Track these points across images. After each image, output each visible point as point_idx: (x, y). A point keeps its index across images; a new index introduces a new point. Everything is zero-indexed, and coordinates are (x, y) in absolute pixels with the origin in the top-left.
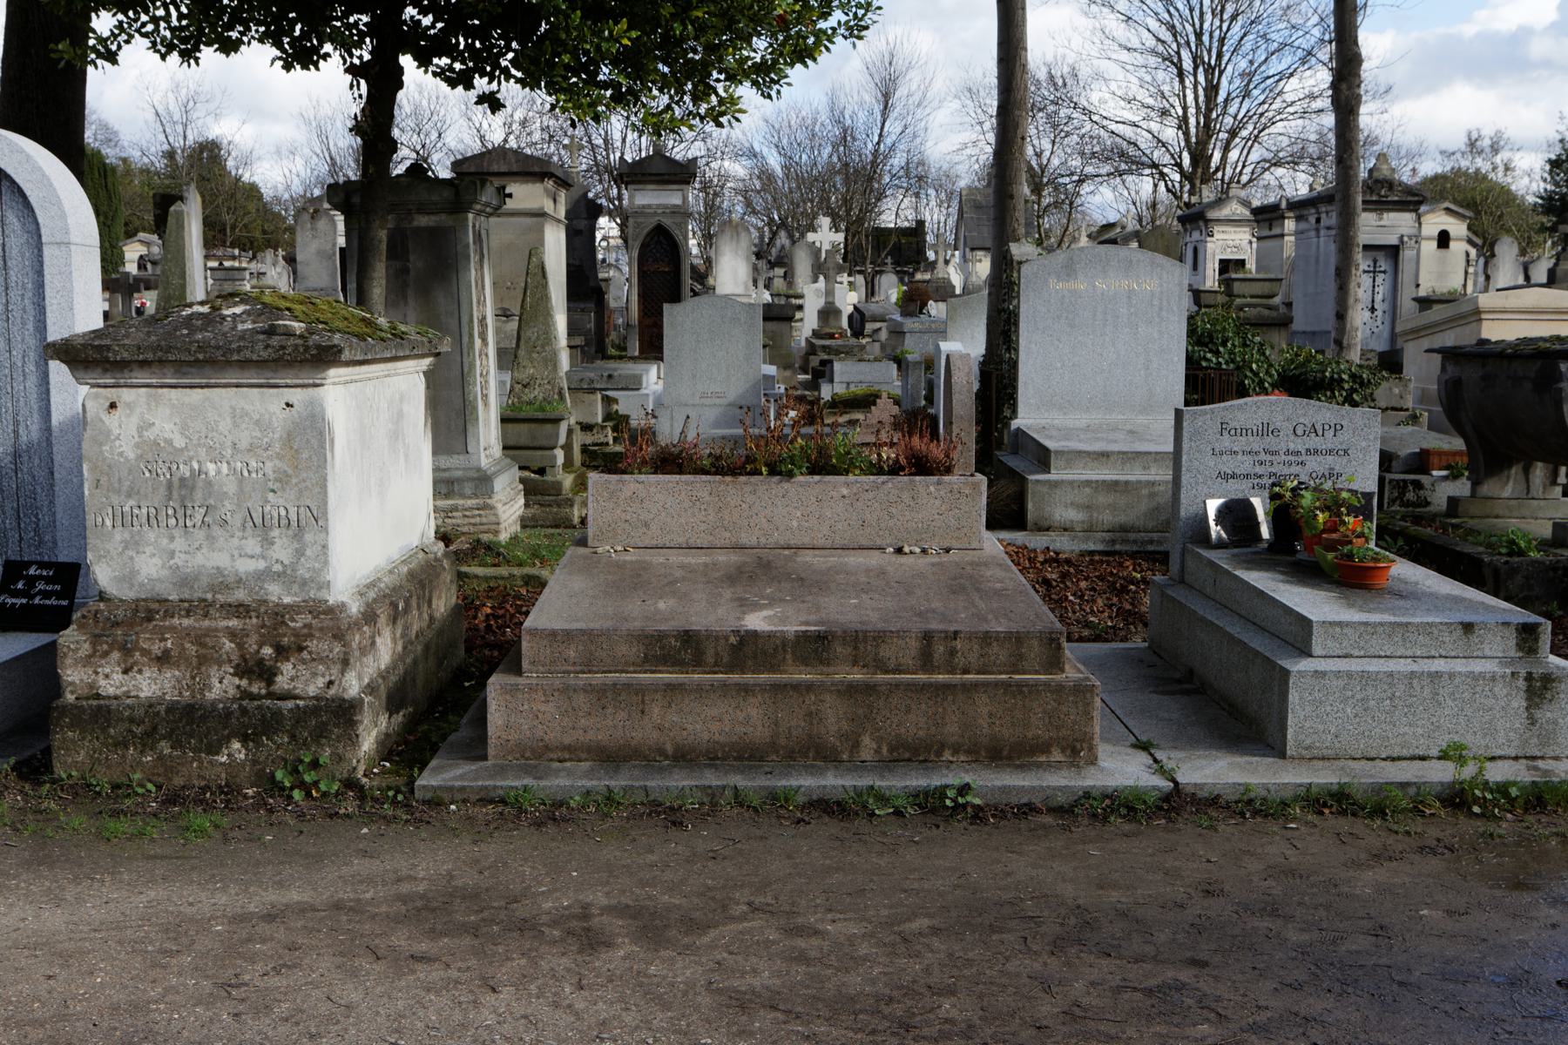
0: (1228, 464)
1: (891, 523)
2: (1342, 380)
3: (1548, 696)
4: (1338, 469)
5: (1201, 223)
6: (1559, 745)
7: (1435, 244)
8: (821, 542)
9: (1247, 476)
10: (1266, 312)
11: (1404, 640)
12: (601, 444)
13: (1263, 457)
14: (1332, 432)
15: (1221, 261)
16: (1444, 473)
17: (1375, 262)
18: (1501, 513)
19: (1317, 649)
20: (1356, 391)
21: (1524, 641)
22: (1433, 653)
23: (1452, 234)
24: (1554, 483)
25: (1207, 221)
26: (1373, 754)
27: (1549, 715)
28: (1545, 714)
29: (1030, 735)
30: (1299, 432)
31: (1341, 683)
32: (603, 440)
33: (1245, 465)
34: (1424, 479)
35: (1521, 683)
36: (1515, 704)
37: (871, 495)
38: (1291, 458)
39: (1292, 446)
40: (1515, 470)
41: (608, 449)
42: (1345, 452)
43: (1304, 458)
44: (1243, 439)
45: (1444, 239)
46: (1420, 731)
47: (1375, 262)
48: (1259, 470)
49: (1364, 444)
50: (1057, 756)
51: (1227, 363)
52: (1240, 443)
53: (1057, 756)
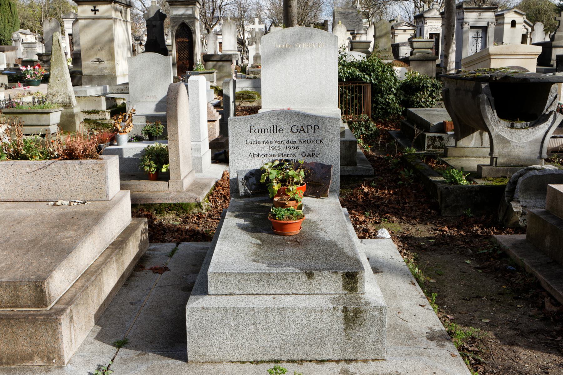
0: (255, 149)
1: (56, 187)
2: (428, 87)
3: (359, 322)
4: (317, 150)
5: (422, 19)
6: (367, 352)
7: (510, 25)
8: (18, 198)
9: (266, 156)
10: (427, 55)
11: (268, 283)
12: (103, 119)
13: (274, 144)
14: (313, 130)
15: (430, 34)
17: (477, 33)
18: (468, 155)
19: (211, 290)
20: (434, 91)
21: (348, 283)
22: (288, 292)
23: (517, 22)
25: (424, 18)
26: (244, 359)
27: (359, 334)
28: (357, 333)
29: (19, 349)
30: (294, 130)
31: (220, 315)
32: (104, 117)
35: (340, 314)
36: (336, 327)
37: (42, 171)
38: (291, 145)
39: (290, 139)
40: (476, 134)
41: (106, 122)
43: (298, 145)
44: (263, 135)
45: (513, 24)
46: (275, 344)
47: (477, 33)
48: (272, 152)
49: (331, 137)
50: (38, 362)
51: (374, 80)
52: (261, 137)
53: (38, 362)
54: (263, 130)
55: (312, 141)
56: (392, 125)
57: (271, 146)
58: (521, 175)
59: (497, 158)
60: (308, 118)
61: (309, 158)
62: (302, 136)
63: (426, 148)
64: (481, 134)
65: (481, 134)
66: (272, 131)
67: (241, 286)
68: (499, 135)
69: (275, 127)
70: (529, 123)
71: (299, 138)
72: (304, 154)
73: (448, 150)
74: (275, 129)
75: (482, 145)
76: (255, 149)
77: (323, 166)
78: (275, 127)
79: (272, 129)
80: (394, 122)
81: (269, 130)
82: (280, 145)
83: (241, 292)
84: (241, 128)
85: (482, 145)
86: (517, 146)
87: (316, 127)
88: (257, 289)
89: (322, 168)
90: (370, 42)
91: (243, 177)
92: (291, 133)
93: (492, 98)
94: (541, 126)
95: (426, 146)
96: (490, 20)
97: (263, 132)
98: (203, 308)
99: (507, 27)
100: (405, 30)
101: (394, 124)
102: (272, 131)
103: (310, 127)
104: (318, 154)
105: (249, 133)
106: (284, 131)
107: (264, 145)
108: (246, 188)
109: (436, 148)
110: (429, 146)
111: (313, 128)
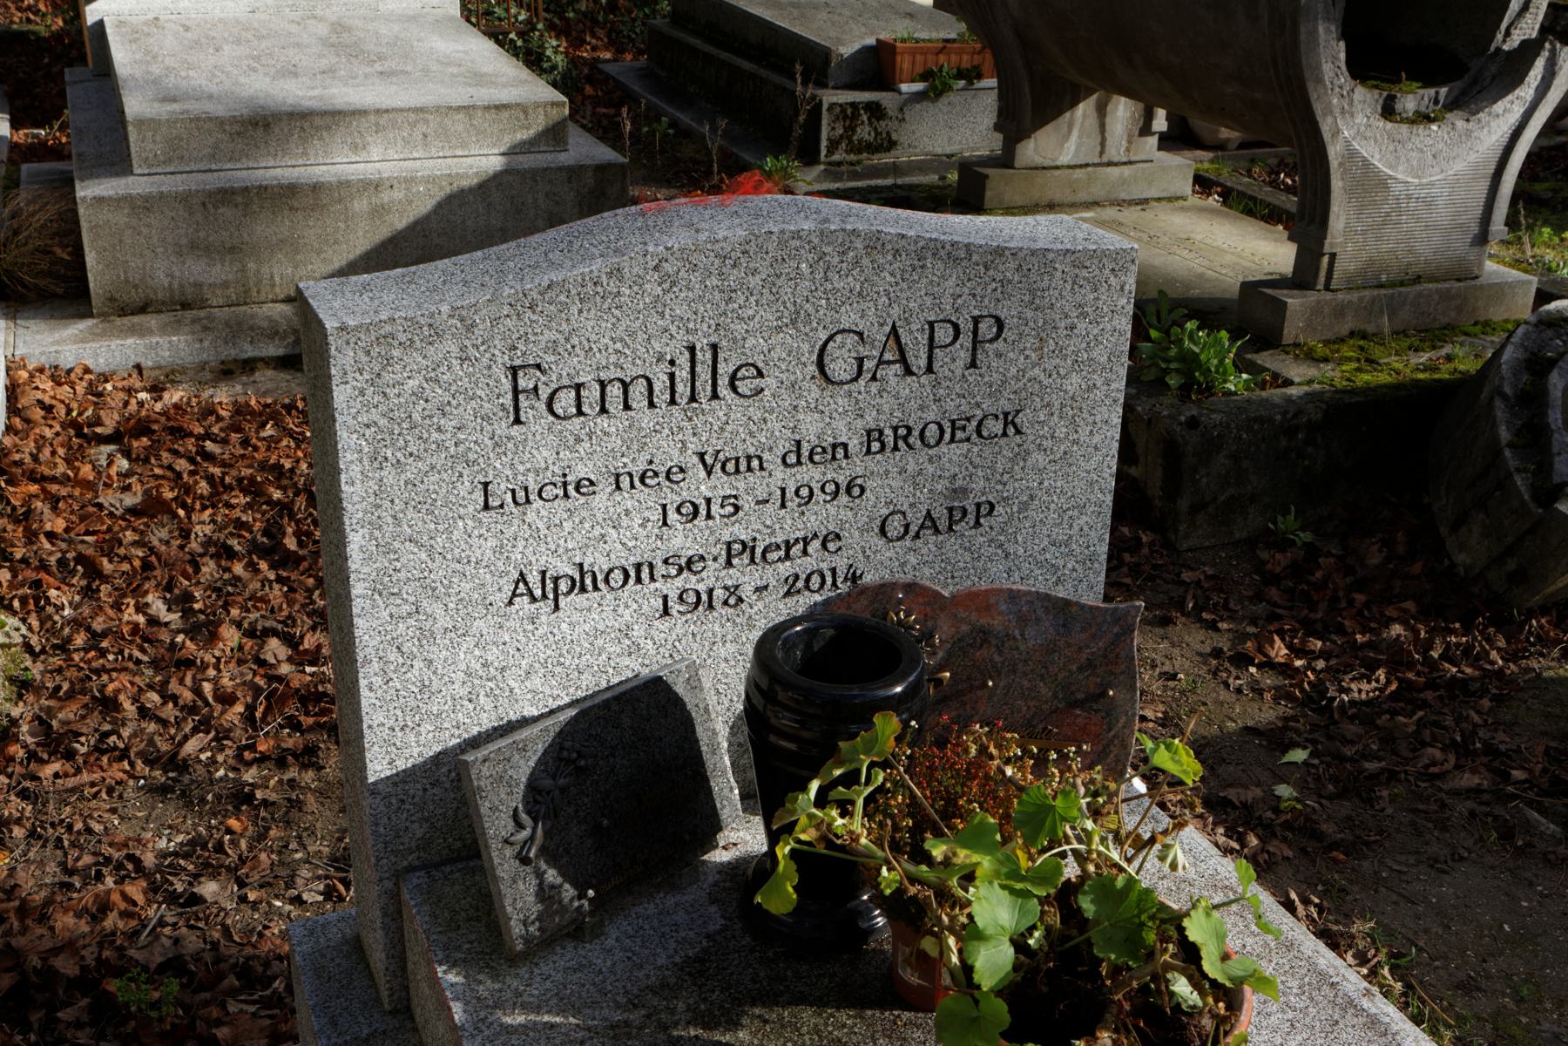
0: (554, 539)
9: (638, 572)
13: (699, 486)
16: (918, 86)
24: (1146, 130)
30: (840, 367)
33: (624, 528)
34: (884, 98)
38: (811, 474)
39: (811, 429)
40: (1084, 110)
42: (1009, 420)
43: (857, 466)
48: (682, 540)
49: (1074, 382)
52: (606, 442)
54: (615, 391)
55: (953, 430)
56: (594, 36)
57: (672, 499)
59: (1333, 256)
60: (934, 267)
62: (887, 403)
63: (823, 152)
64: (1101, 110)
65: (1101, 110)
66: (682, 389)
68: (1352, 154)
69: (704, 356)
70: (1444, 91)
71: (870, 420)
73: (989, 184)
74: (704, 373)
75: (1102, 153)
76: (554, 539)
78: (704, 356)
79: (683, 374)
80: (595, 22)
81: (661, 383)
84: (438, 394)
85: (1102, 153)
86: (1409, 197)
91: (517, 800)
92: (813, 392)
94: (1499, 107)
95: (824, 143)
97: (615, 404)
101: (601, 33)
102: (682, 389)
103: (943, 334)
105: (502, 427)
106: (770, 382)
107: (627, 500)
108: (552, 875)
109: (860, 152)
110: (833, 145)
111: (966, 340)
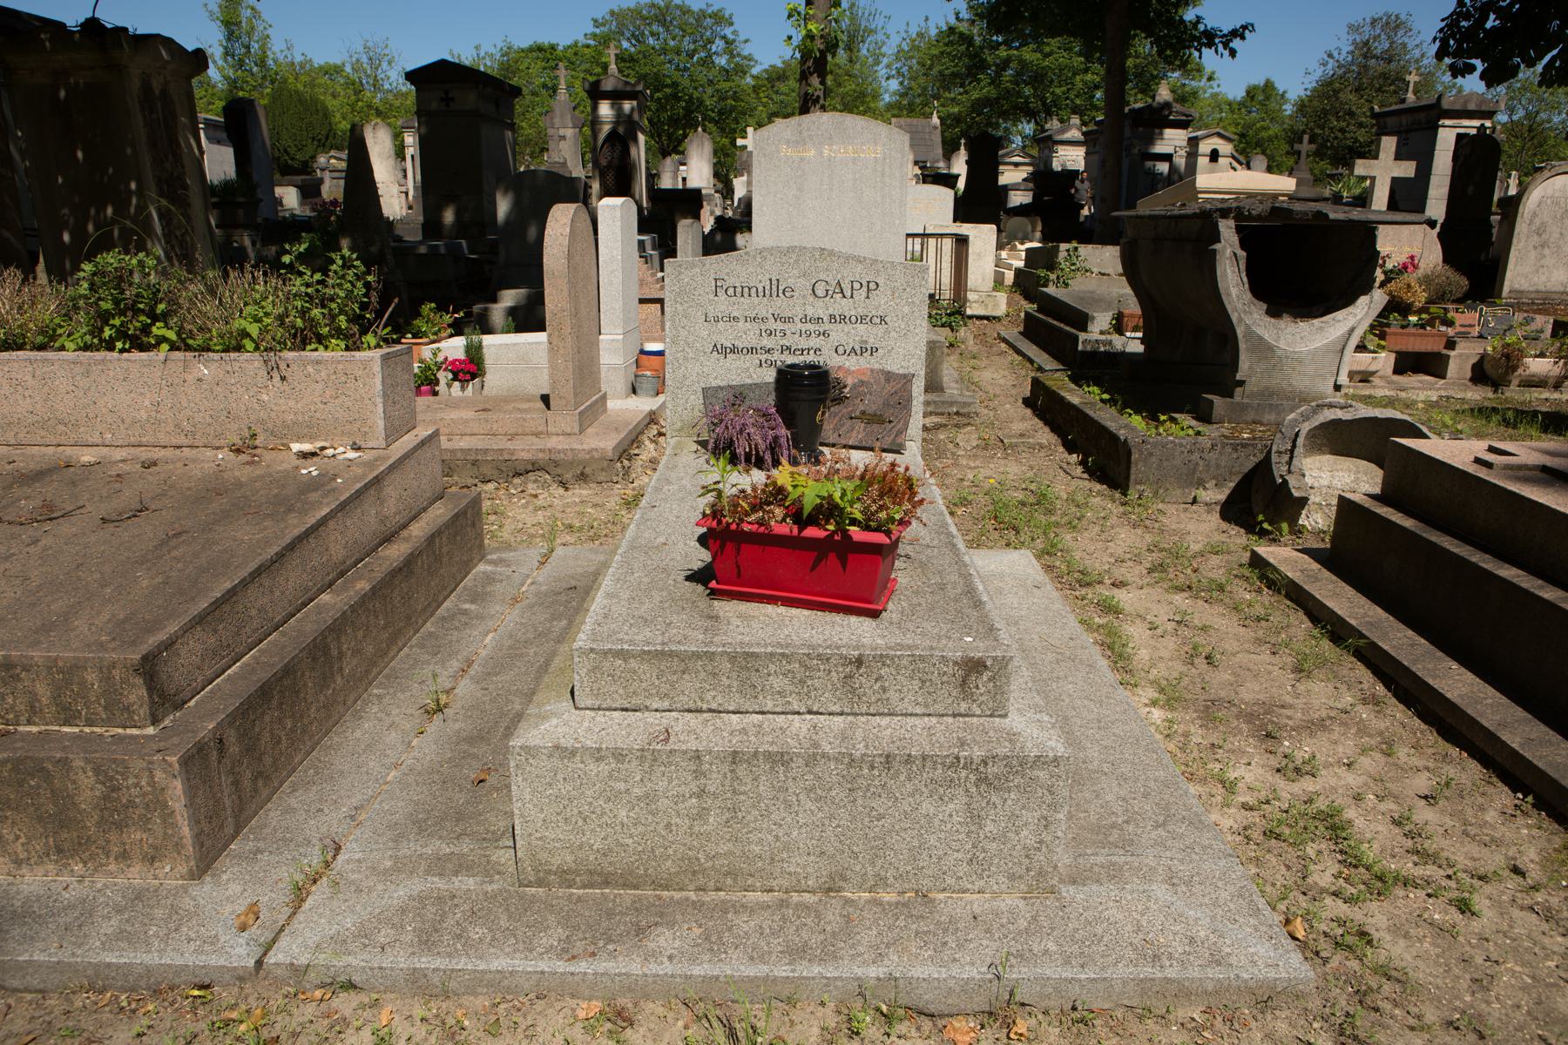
9: (751, 350)
38: (809, 326)
43: (827, 326)
48: (767, 342)
55: (861, 319)
58: (1306, 418)
61: (853, 358)
67: (665, 688)
71: (831, 311)
72: (841, 350)
77: (889, 376)
82: (786, 326)
83: (666, 704)
87: (872, 286)
88: (709, 696)
89: (888, 380)
90: (957, 176)
93: (1242, 254)
96: (1178, 143)
98: (557, 747)
99: (1203, 161)
100: (1016, 165)
103: (856, 286)
104: (874, 350)
105: (712, 297)
